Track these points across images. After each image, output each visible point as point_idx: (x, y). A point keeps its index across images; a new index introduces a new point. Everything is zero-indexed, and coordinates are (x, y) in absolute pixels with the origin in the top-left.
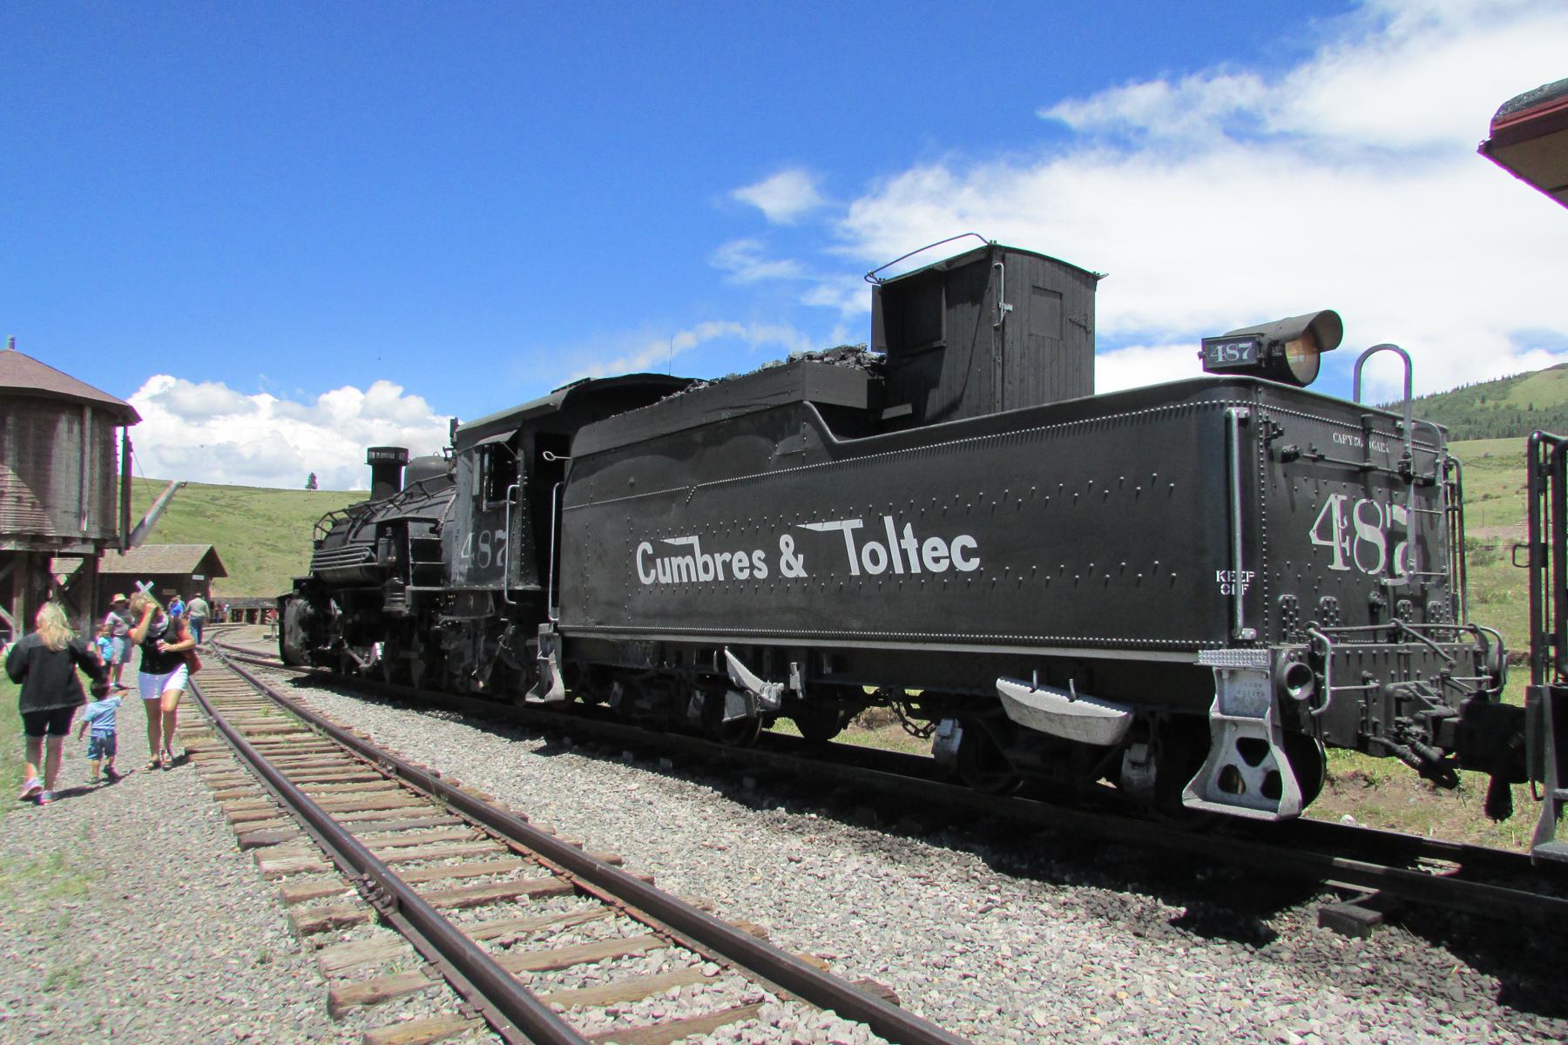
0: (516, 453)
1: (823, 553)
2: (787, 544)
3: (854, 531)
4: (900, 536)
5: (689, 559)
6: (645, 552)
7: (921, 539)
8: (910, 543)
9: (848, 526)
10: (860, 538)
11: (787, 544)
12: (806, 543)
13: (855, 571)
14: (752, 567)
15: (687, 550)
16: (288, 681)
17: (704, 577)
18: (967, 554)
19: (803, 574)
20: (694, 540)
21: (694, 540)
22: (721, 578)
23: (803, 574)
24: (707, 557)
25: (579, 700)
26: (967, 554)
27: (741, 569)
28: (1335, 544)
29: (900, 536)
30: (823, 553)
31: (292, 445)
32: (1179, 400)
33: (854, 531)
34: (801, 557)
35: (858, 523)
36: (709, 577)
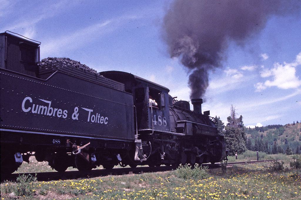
0: (212, 126)
1: (83, 115)
2: (76, 110)
3: (91, 112)
4: (98, 115)
5: (46, 107)
6: (106, 119)
7: (101, 117)
8: (99, 117)
9: (90, 111)
10: (92, 114)
11: (76, 110)
12: (81, 111)
13: (88, 121)
14: (63, 114)
15: (47, 105)
16: (294, 122)
17: (48, 114)
18: (106, 121)
19: (77, 119)
20: (50, 102)
21: (50, 102)
22: (54, 115)
23: (77, 119)
24: (52, 108)
25: (159, 93)
26: (106, 121)
27: (59, 115)
28: (153, 130)
29: (98, 115)
30: (83, 115)
31: (265, 132)
32: (135, 115)
33: (91, 112)
34: (78, 114)
35: (92, 111)
36: (50, 115)
